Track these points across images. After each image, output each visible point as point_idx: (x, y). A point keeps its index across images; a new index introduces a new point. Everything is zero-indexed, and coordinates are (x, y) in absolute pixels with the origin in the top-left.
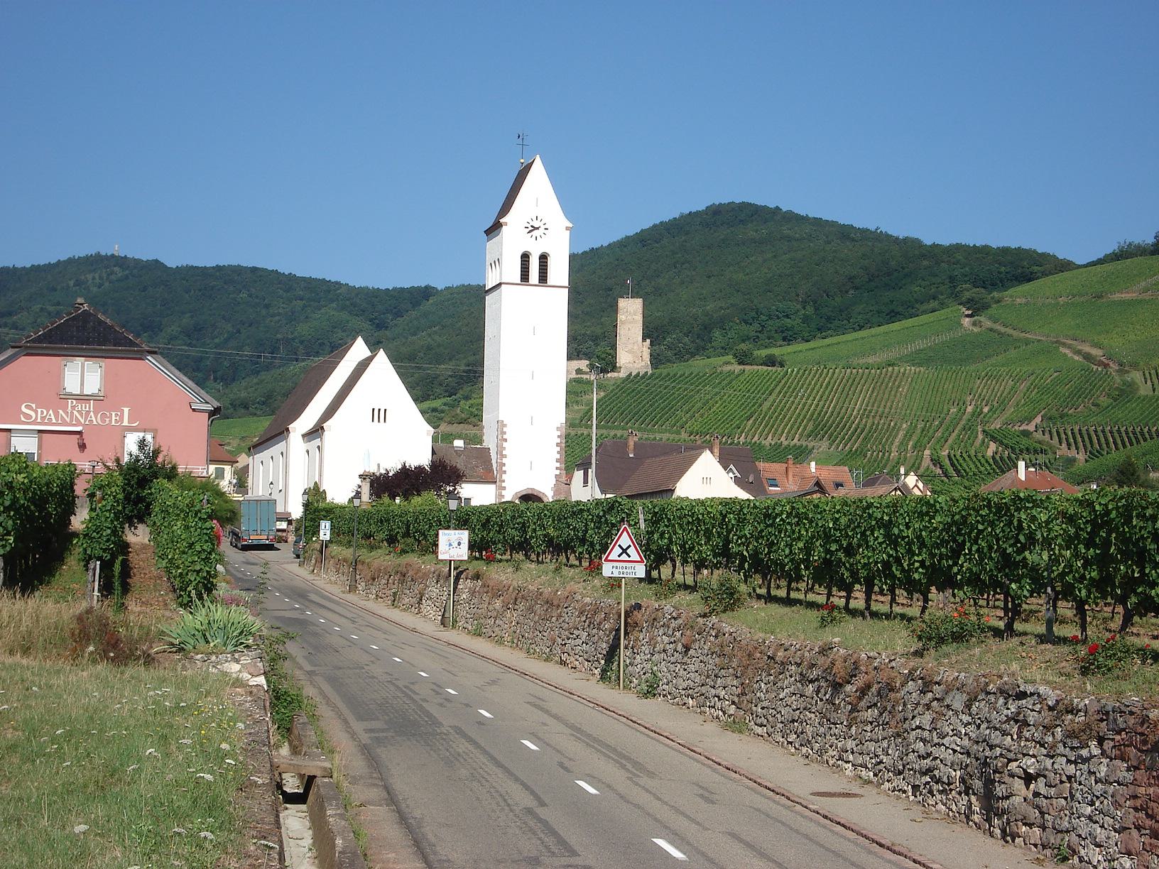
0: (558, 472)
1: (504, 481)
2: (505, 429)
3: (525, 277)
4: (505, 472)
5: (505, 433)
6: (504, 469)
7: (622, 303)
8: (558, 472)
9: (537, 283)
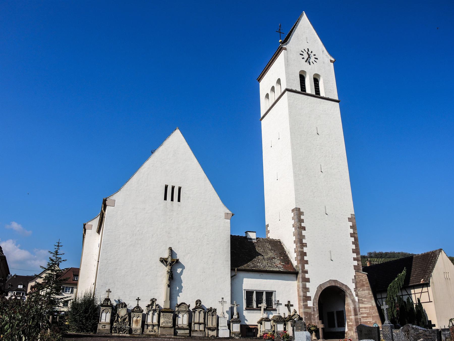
0: (356, 263)
1: (307, 272)
2: (302, 217)
4: (307, 262)
6: (306, 258)
8: (356, 263)
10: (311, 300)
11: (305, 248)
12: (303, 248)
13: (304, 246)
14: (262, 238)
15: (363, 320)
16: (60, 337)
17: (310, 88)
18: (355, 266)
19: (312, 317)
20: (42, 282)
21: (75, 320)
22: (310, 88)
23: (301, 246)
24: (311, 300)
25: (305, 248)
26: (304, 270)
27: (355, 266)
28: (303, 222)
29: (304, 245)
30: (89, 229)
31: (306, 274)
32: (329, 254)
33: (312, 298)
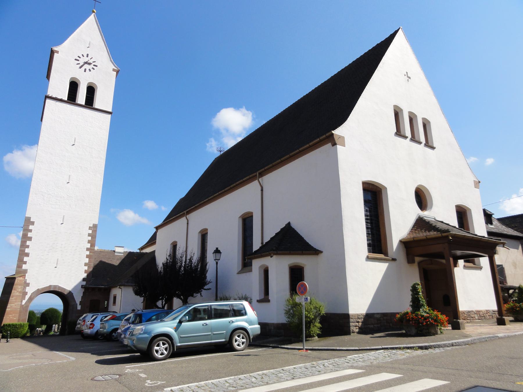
3: (72, 98)
5: (89, 242)
7: (116, 292)
9: (84, 103)
17: (81, 97)
22: (81, 97)
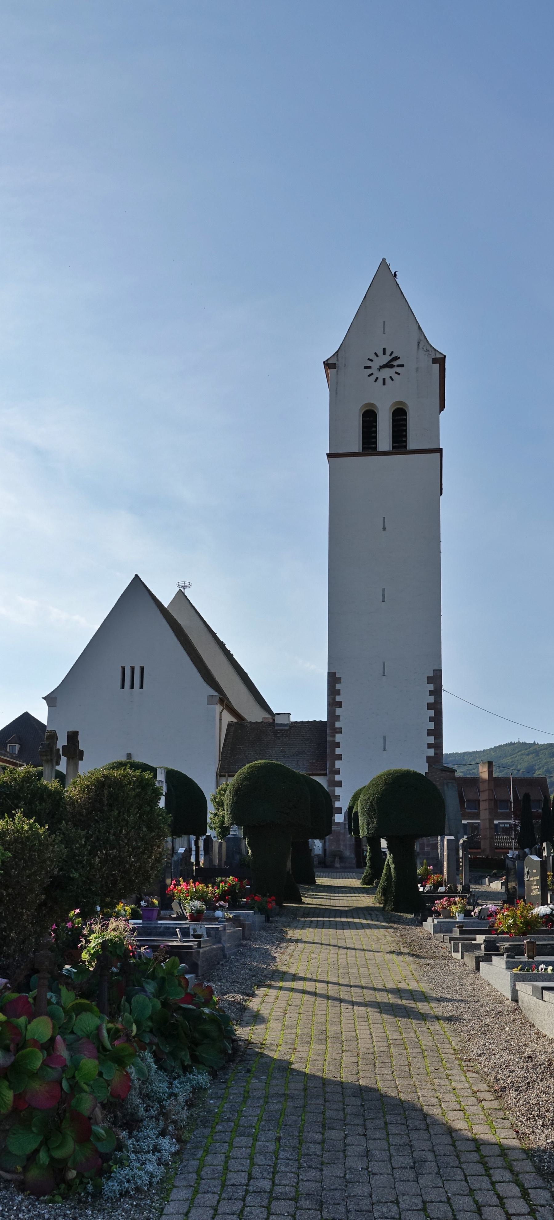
2: (338, 686)
10: (341, 813)
11: (337, 736)
12: (335, 736)
13: (338, 733)
14: (111, 768)
15: (433, 841)
16: (72, 923)
17: (384, 441)
18: (428, 757)
19: (342, 837)
20: (82, 751)
21: (441, 997)
22: (384, 441)
23: (331, 733)
24: (341, 813)
25: (337, 736)
26: (334, 769)
27: (428, 757)
28: (339, 694)
29: (338, 730)
30: (422, 338)
31: (336, 776)
32: (382, 741)
33: (344, 811)
